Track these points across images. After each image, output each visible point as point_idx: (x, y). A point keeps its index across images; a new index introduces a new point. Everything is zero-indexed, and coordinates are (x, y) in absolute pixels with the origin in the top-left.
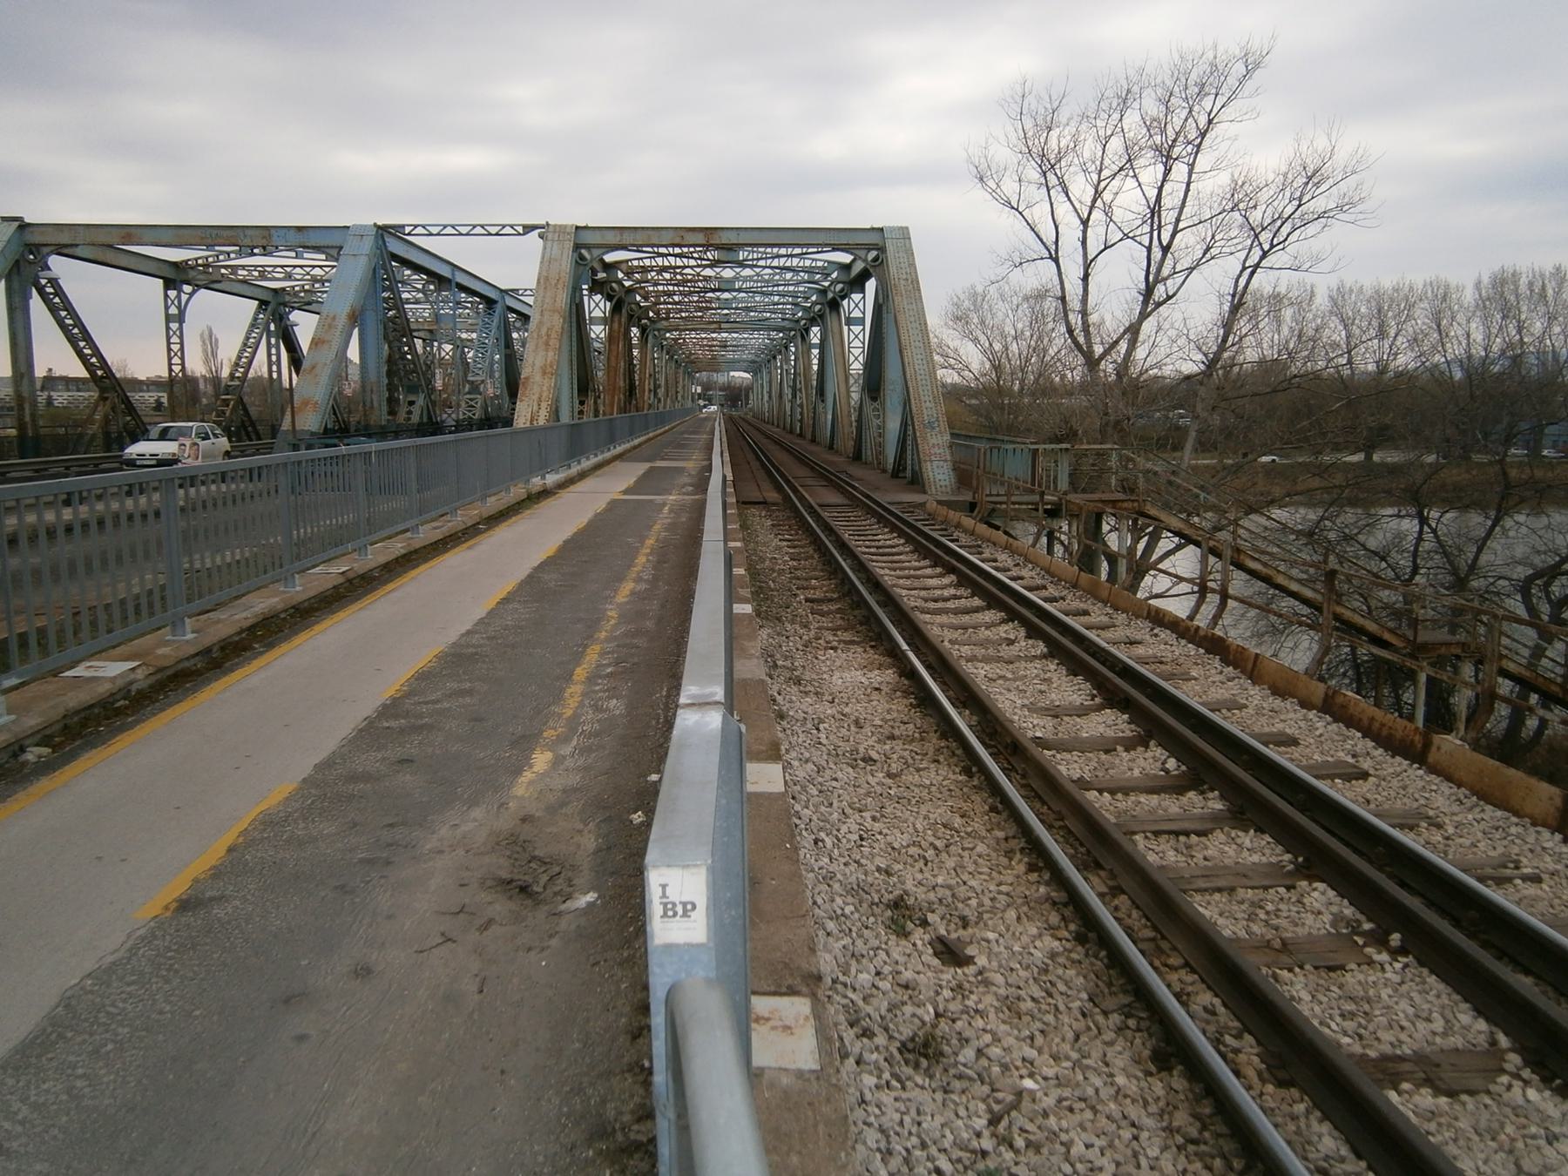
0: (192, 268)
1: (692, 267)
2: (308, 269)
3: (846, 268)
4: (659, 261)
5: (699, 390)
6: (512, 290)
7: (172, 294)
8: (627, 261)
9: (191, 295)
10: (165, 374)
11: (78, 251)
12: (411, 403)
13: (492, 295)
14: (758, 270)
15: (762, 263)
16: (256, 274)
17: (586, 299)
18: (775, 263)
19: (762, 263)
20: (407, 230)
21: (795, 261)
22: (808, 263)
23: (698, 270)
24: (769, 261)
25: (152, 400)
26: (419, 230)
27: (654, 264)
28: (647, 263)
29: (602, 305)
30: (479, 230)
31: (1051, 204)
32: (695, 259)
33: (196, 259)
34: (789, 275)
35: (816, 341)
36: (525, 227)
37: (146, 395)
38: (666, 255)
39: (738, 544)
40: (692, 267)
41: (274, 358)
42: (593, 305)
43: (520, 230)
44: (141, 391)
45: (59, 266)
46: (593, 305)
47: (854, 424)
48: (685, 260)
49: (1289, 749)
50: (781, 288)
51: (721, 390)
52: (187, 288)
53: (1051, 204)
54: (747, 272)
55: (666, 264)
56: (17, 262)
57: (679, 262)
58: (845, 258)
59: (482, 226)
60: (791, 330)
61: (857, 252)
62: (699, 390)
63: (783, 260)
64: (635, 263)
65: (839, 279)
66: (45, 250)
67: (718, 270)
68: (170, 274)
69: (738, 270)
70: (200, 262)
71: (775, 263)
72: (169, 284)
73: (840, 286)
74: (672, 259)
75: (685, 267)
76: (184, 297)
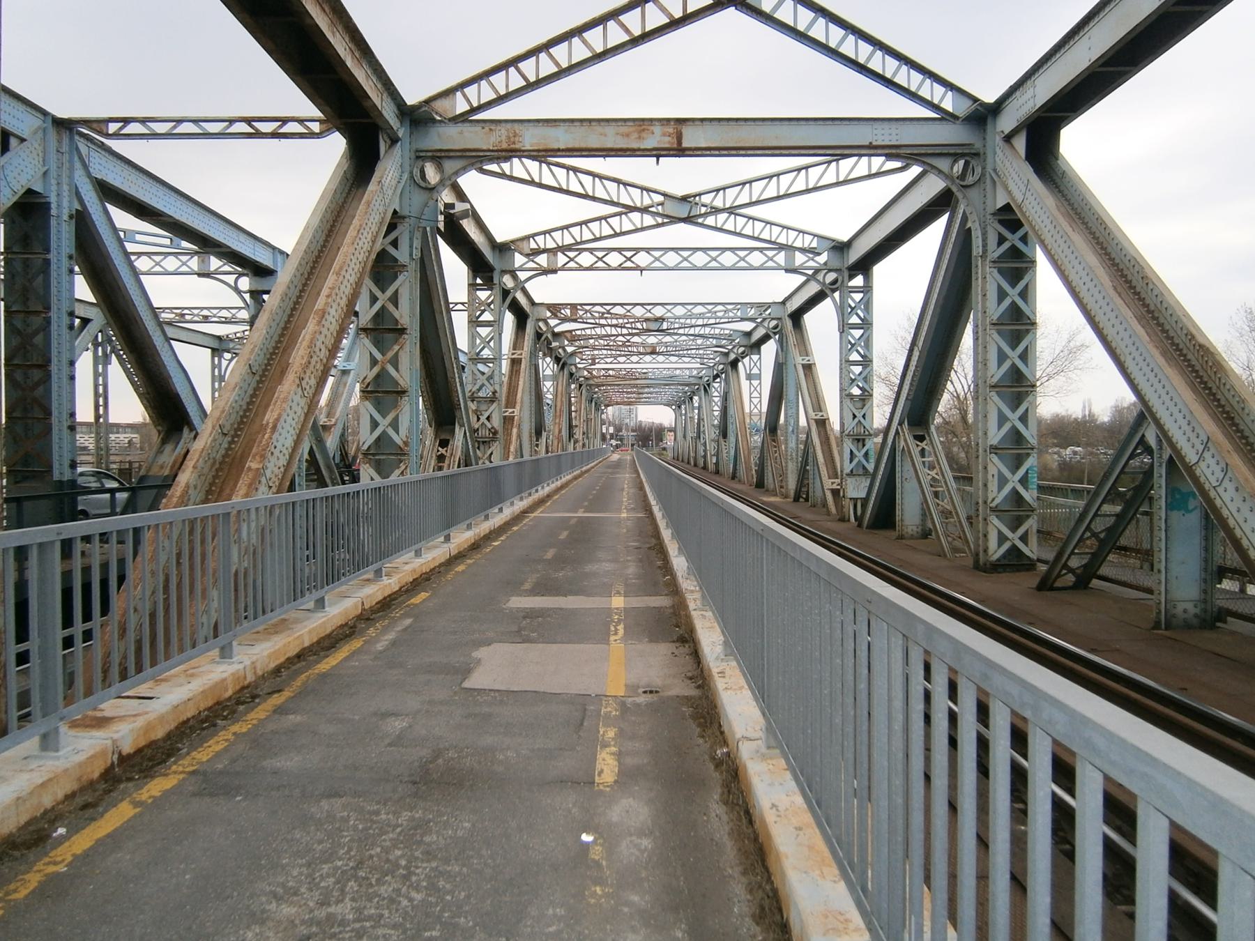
0: (232, 340)
1: (623, 335)
3: (748, 334)
4: (598, 331)
5: (611, 430)
6: (86, 122)
8: (570, 331)
13: (264, 258)
14: (676, 337)
15: (681, 331)
17: (540, 361)
18: (692, 331)
19: (681, 331)
20: (113, 128)
21: (707, 330)
22: (717, 331)
23: (628, 338)
24: (687, 330)
25: (126, 440)
27: (594, 333)
28: (588, 332)
29: (551, 365)
30: (244, 128)
32: (628, 328)
33: (244, 332)
34: (699, 341)
35: (696, 405)
37: (122, 436)
38: (603, 326)
40: (623, 335)
41: (101, 390)
42: (545, 365)
44: (118, 433)
46: (545, 365)
47: (754, 468)
48: (619, 329)
50: (693, 352)
51: (633, 431)
54: (668, 339)
55: (604, 333)
57: (614, 332)
58: (748, 326)
60: (695, 385)
61: (929, 160)
62: (611, 430)
63: (698, 329)
64: (578, 333)
65: (831, 265)
67: (644, 337)
68: (215, 345)
69: (660, 337)
70: (238, 335)
71: (692, 331)
72: (216, 352)
73: (742, 349)
74: (608, 329)
75: (617, 336)
76: (224, 363)
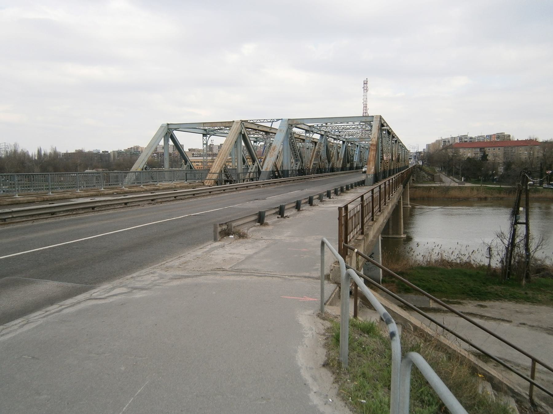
2: (351, 126)
7: (205, 138)
9: (209, 137)
10: (202, 149)
11: (180, 129)
12: (296, 164)
16: (336, 128)
26: (258, 121)
31: (452, 332)
36: (277, 120)
39: (62, 178)
43: (276, 120)
45: (175, 133)
49: (183, 274)
52: (208, 136)
53: (452, 332)
56: (167, 133)
59: (252, 120)
66: (173, 130)
72: (204, 135)
